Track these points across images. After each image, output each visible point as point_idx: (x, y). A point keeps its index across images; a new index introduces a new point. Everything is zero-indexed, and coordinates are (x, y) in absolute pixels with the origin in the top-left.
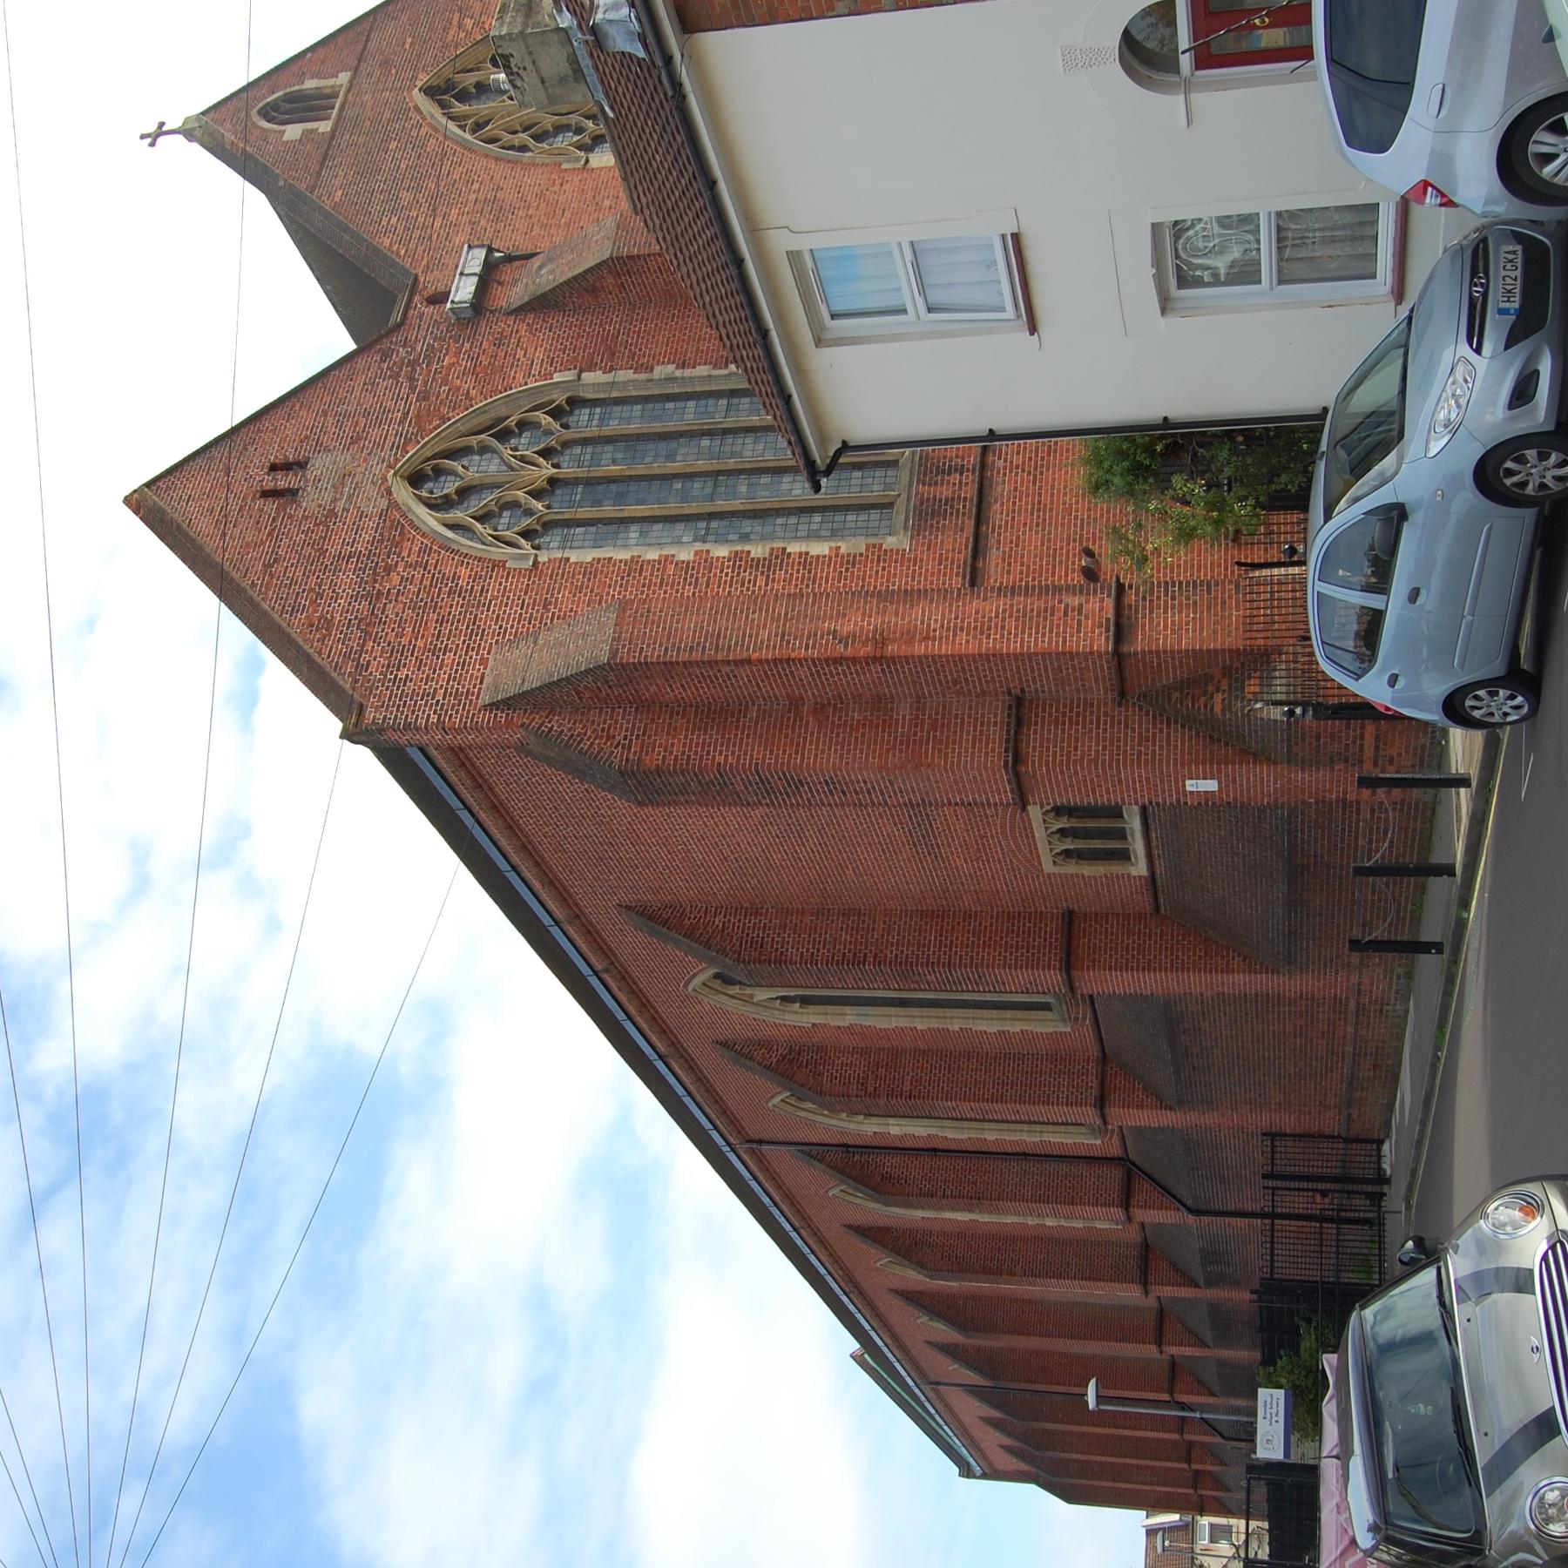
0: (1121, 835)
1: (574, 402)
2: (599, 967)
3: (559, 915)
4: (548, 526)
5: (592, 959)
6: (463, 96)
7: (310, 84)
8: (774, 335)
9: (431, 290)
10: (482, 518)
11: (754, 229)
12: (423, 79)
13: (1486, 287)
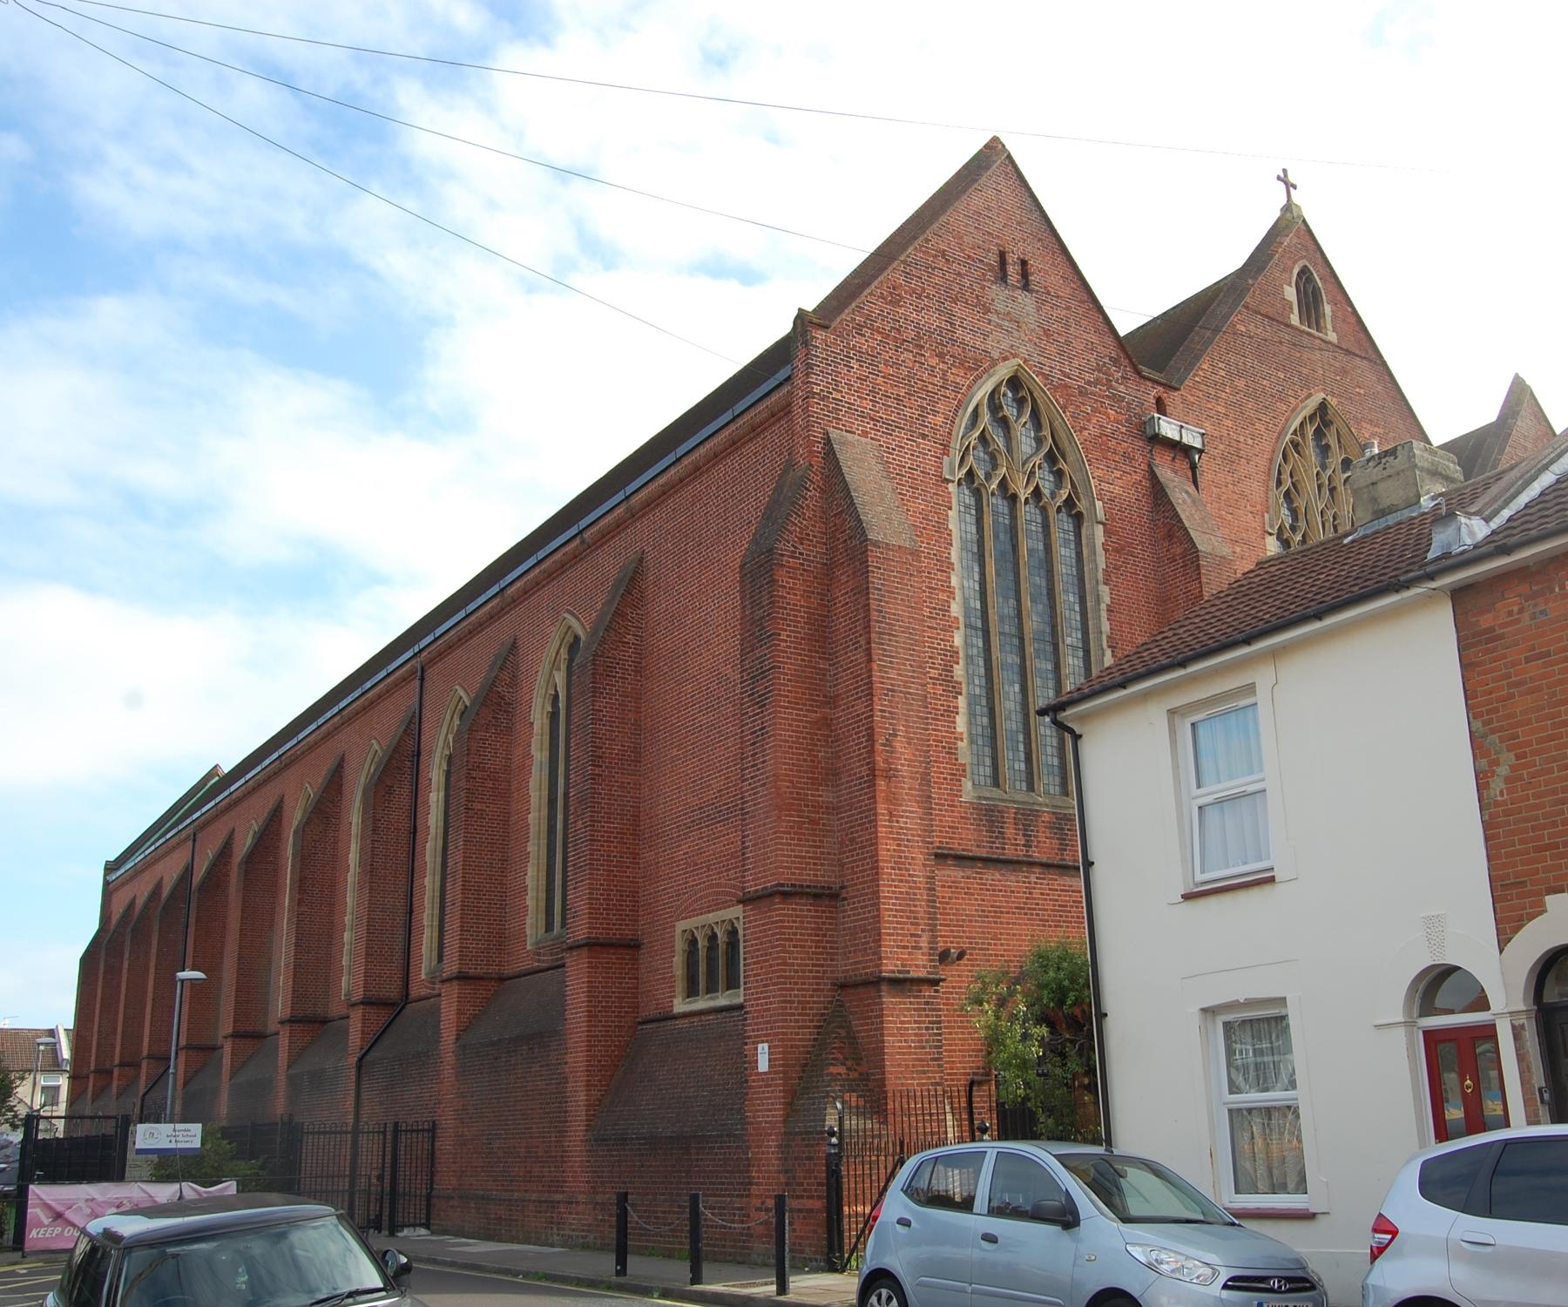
0: (711, 989)
1: (1078, 518)
2: (586, 535)
3: (635, 500)
4: (977, 493)
5: (594, 529)
6: (1319, 434)
7: (1328, 309)
8: (1181, 672)
9: (1167, 402)
10: (983, 438)
11: (1275, 654)
12: (1333, 401)
13: (1278, 1291)
